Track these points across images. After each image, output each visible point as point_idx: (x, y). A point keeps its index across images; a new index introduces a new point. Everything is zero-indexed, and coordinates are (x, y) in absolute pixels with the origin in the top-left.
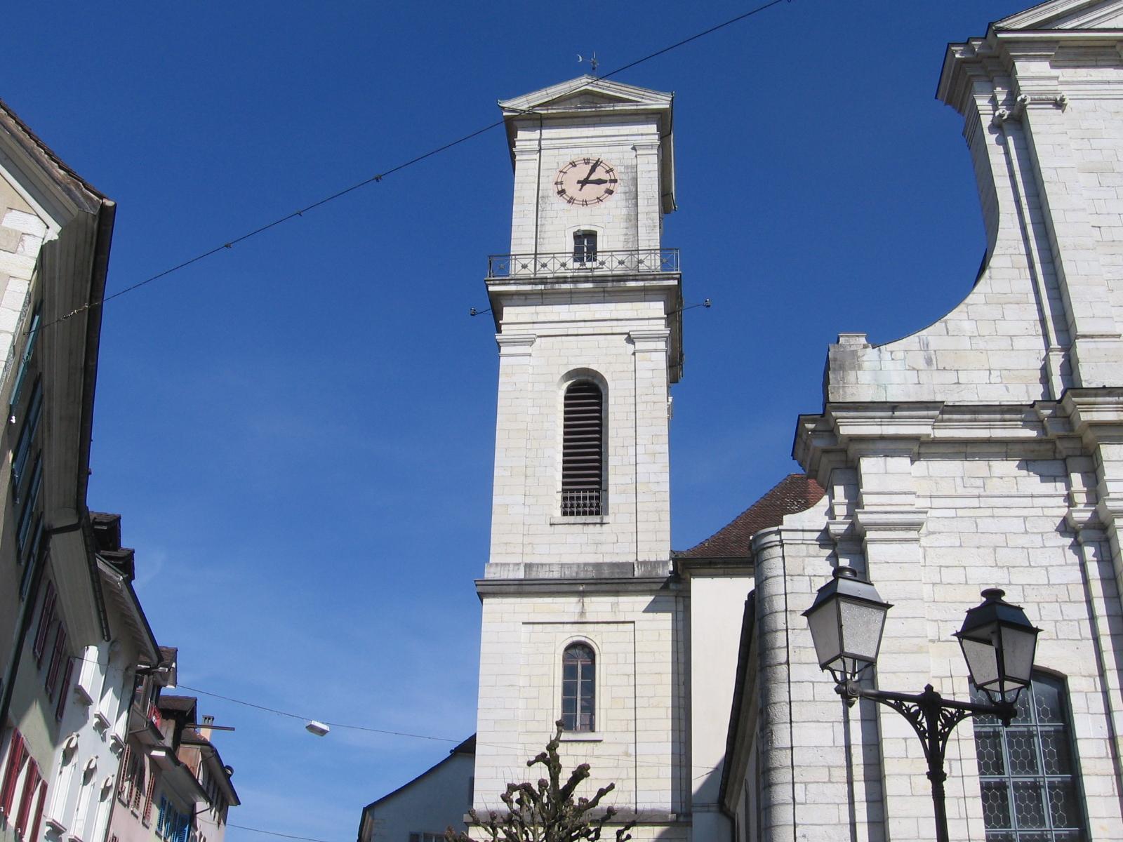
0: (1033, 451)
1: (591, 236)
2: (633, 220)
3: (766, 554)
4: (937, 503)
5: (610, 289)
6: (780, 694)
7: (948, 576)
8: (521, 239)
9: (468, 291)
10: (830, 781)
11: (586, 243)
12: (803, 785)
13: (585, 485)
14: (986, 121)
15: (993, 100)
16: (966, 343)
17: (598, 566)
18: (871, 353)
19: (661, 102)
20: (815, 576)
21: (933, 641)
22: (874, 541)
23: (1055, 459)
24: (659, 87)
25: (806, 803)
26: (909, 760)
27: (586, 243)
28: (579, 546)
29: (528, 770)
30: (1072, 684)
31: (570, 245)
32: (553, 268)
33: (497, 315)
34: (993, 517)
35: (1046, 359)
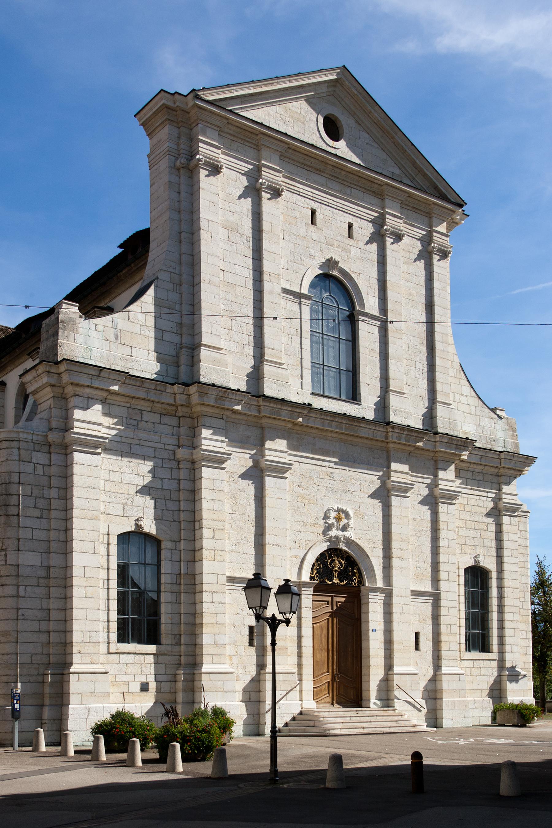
0: (165, 409)
10: (38, 586)
12: (24, 587)
16: (137, 329)
18: (84, 324)
20: (37, 464)
21: (102, 513)
23: (175, 416)
25: (25, 597)
26: (85, 579)
29: (109, 670)
30: (164, 545)
34: (140, 445)
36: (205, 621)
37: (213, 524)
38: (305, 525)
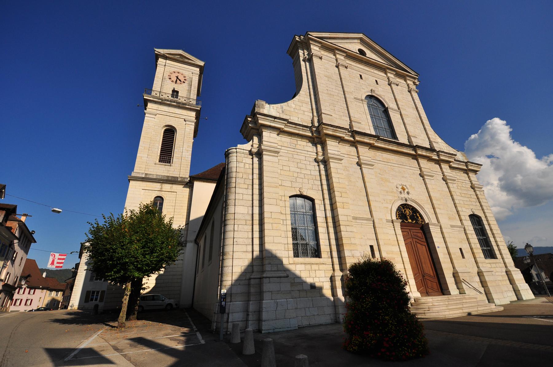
1: (177, 92)
2: (190, 91)
3: (231, 155)
4: (283, 148)
5: (181, 106)
6: (232, 197)
7: (285, 168)
8: (156, 86)
9: (137, 94)
11: (175, 93)
13: (166, 154)
14: (301, 59)
15: (304, 54)
17: (168, 177)
19: (202, 63)
22: (265, 154)
24: (202, 60)
27: (175, 93)
28: (163, 170)
30: (316, 202)
31: (171, 92)
32: (165, 97)
33: (146, 105)
35: (313, 118)
36: (344, 242)
37: (340, 190)
38: (387, 192)
